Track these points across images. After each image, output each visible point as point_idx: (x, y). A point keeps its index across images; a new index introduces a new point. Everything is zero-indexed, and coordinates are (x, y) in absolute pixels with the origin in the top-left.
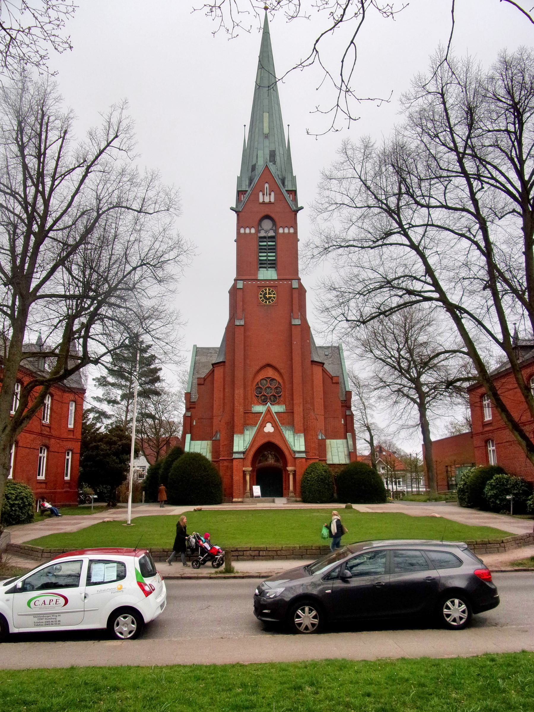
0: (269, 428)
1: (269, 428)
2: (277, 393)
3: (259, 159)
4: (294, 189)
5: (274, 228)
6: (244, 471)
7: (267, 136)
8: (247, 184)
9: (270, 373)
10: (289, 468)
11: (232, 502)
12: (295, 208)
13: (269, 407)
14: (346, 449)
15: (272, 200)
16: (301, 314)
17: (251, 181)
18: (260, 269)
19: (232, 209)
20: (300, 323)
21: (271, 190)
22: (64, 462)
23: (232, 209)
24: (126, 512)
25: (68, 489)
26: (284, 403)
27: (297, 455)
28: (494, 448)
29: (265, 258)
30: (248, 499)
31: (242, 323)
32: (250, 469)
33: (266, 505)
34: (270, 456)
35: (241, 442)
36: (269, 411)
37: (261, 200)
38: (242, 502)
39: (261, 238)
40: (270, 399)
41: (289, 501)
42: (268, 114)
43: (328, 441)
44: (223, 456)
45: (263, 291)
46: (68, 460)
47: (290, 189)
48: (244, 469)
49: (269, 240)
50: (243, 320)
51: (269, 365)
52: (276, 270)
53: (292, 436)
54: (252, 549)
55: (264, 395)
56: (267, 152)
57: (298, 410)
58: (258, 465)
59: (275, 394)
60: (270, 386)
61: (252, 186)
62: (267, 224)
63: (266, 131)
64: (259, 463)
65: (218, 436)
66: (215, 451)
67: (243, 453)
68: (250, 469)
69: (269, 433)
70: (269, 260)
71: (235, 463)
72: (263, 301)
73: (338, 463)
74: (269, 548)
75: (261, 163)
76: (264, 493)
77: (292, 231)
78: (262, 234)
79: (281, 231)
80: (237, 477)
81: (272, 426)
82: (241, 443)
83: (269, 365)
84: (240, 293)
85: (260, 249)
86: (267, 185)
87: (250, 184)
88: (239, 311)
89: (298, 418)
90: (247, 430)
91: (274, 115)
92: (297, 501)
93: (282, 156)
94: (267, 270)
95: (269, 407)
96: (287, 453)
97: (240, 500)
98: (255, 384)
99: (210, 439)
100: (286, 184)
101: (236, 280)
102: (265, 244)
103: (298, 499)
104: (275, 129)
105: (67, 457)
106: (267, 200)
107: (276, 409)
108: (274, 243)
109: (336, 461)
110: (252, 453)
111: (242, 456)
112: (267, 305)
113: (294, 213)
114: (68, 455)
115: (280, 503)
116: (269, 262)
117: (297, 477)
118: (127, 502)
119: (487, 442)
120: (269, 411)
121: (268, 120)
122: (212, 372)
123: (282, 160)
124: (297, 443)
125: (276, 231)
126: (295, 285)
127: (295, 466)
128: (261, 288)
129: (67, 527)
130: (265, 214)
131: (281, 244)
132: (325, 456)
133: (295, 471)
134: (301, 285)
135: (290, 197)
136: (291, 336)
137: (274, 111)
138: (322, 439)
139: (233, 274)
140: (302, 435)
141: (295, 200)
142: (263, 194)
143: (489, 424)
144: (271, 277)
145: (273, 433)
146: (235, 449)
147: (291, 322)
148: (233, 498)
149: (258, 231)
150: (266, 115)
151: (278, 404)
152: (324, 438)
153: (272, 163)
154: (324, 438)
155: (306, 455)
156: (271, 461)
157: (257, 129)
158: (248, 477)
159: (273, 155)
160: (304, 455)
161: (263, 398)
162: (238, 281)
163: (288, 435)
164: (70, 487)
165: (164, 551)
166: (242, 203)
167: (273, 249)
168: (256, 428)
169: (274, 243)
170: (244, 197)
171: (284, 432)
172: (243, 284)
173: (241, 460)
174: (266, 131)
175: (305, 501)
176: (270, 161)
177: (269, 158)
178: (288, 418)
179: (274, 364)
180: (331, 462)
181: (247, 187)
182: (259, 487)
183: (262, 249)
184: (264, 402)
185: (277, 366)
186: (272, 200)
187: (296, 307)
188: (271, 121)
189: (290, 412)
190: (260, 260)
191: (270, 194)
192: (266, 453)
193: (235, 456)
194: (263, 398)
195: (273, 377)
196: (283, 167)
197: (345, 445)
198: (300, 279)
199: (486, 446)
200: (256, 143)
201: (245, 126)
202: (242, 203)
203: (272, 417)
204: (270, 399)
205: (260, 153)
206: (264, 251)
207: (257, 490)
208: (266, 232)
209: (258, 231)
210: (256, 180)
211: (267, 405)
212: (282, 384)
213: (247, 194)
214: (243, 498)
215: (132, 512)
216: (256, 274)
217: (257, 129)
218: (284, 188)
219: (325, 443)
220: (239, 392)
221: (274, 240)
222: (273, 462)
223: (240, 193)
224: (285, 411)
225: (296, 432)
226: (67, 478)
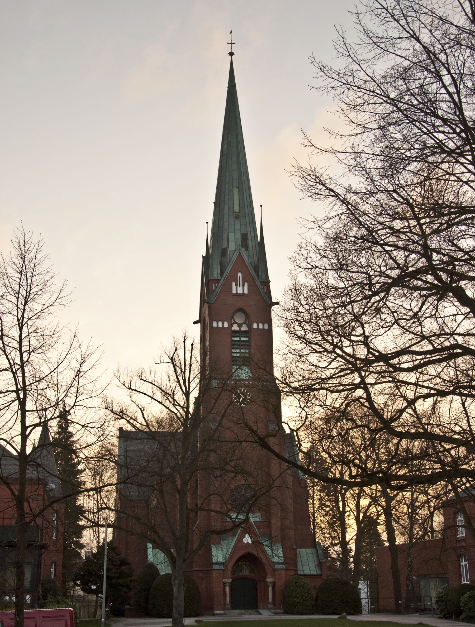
0: (247, 539)
3: (230, 243)
5: (247, 322)
7: (237, 216)
8: (219, 272)
10: (269, 580)
11: (214, 614)
14: (316, 559)
27: (277, 567)
28: (467, 563)
34: (245, 567)
37: (234, 291)
38: (224, 614)
48: (224, 580)
56: (239, 235)
61: (224, 275)
63: (237, 209)
68: (230, 580)
71: (215, 575)
77: (266, 327)
78: (235, 327)
79: (255, 326)
82: (219, 555)
89: (276, 528)
97: (222, 612)
100: (260, 274)
102: (238, 339)
103: (280, 611)
106: (240, 291)
108: (247, 339)
109: (307, 572)
110: (231, 564)
111: (222, 567)
119: (459, 557)
124: (276, 555)
125: (250, 326)
127: (274, 578)
133: (274, 583)
142: (236, 285)
143: (463, 540)
153: (244, 249)
156: (246, 572)
168: (235, 539)
169: (247, 339)
173: (221, 572)
174: (237, 209)
175: (287, 612)
176: (243, 247)
180: (302, 573)
181: (219, 275)
183: (234, 345)
186: (246, 292)
188: (241, 199)
189: (267, 522)
190: (233, 357)
191: (243, 285)
199: (459, 562)
205: (231, 236)
206: (236, 347)
209: (231, 325)
214: (224, 610)
224: (261, 520)
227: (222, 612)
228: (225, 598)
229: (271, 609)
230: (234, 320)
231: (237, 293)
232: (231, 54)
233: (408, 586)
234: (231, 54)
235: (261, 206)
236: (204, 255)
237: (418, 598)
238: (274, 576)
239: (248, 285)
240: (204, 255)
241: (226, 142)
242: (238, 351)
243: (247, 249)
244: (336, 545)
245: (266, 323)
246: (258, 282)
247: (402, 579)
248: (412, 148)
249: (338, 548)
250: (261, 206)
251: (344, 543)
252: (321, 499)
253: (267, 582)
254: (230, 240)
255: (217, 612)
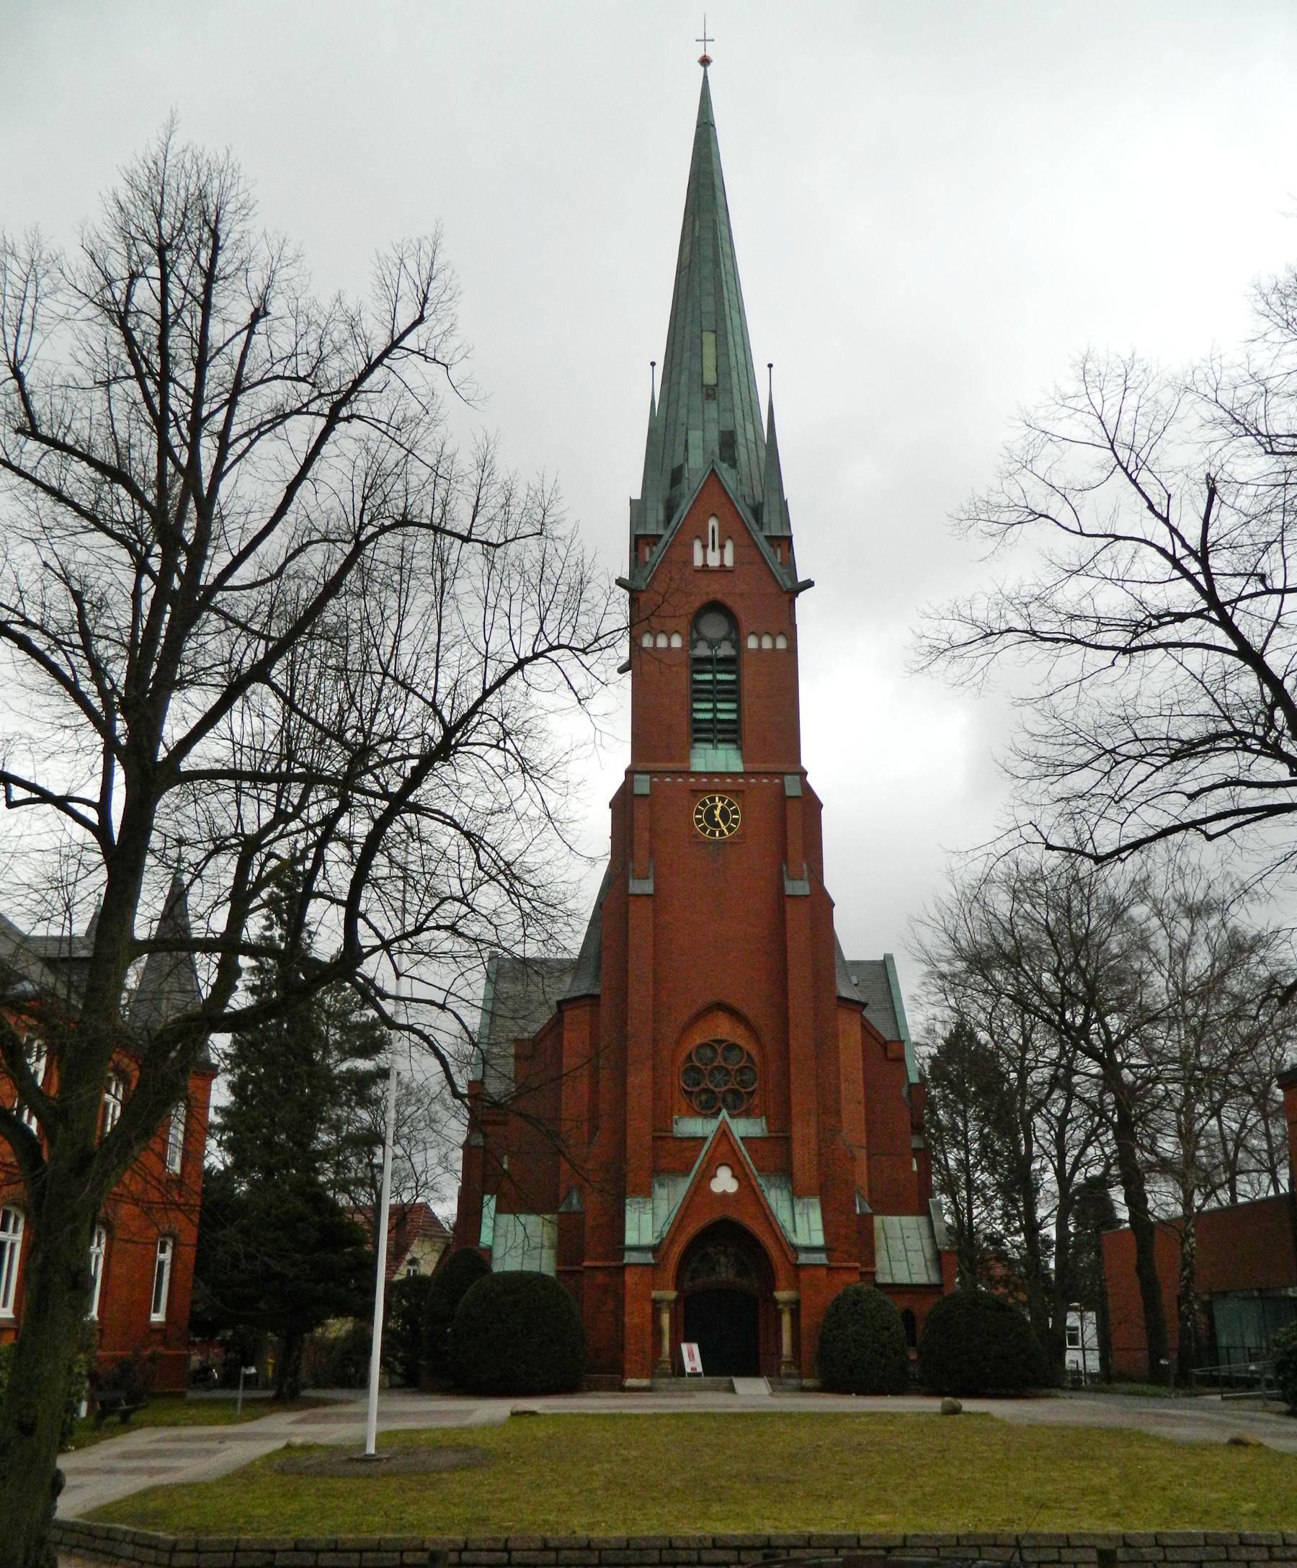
0: (724, 1182)
1: (724, 1182)
2: (743, 1084)
3: (692, 452)
4: (786, 534)
5: (733, 636)
6: (655, 1302)
7: (710, 393)
8: (661, 516)
9: (724, 1028)
10: (782, 1295)
12: (789, 584)
13: (724, 1122)
14: (927, 1242)
15: (729, 562)
16: (810, 870)
17: (670, 509)
18: (697, 745)
19: (620, 582)
20: (807, 892)
21: (725, 535)
22: (149, 1267)
23: (620, 582)
24: (363, 1417)
25: (161, 1350)
26: (764, 1112)
27: (803, 1258)
29: (709, 716)
30: (666, 1380)
31: (647, 887)
32: (672, 1295)
33: (711, 1401)
34: (723, 1260)
35: (647, 1218)
36: (724, 1133)
37: (698, 562)
39: (699, 660)
40: (724, 1100)
41: (778, 1386)
42: (712, 336)
43: (878, 1220)
44: (595, 1259)
45: (704, 804)
46: (162, 1264)
47: (776, 532)
48: (655, 1294)
49: (721, 668)
50: (651, 880)
51: (721, 1007)
52: (740, 748)
53: (787, 1204)
54: (815, 1544)
55: (707, 1090)
56: (713, 435)
57: (804, 1132)
58: (687, 1284)
59: (736, 1086)
60: (723, 1064)
61: (673, 523)
62: (714, 627)
63: (710, 377)
64: (692, 1279)
65: (575, 1201)
66: (569, 1245)
67: (654, 1249)
68: (672, 1295)
69: (725, 1194)
70: (708, 701)
71: (630, 1278)
72: (704, 829)
73: (906, 1281)
74: (869, 1537)
75: (696, 462)
76: (714, 1365)
78: (702, 650)
79: (752, 643)
80: (635, 1316)
81: (734, 1176)
82: (644, 1224)
83: (721, 1007)
84: (641, 814)
85: (696, 691)
86: (713, 523)
87: (668, 519)
88: (641, 853)
89: (803, 1156)
90: (661, 1185)
91: (730, 337)
92: (803, 1389)
93: (752, 446)
94: (715, 748)
95: (724, 1122)
96: (774, 1253)
97: (645, 1382)
98: (684, 1055)
99: (553, 1210)
100: (765, 519)
101: (629, 773)
102: (709, 677)
104: (734, 374)
105: (161, 1256)
106: (713, 560)
107: (742, 1128)
109: (902, 1277)
110: (677, 1250)
111: (649, 1258)
112: (717, 841)
113: (787, 598)
114: (163, 1251)
115: (752, 1392)
116: (719, 727)
117: (804, 1323)
118: (363, 1383)
120: (724, 1133)
121: (713, 349)
122: (557, 1023)
123: (754, 457)
124: (805, 1226)
125: (738, 644)
126: (792, 789)
128: (700, 795)
129: (182, 1463)
130: (705, 598)
131: (752, 679)
132: (872, 1263)
133: (798, 1302)
134: (807, 789)
135: (775, 553)
136: (783, 922)
137: (729, 329)
138: (863, 1215)
139: (622, 758)
140: (816, 1201)
141: (790, 564)
142: (705, 547)
144: (727, 766)
145: (735, 1194)
146: (631, 1238)
147: (781, 887)
148: (623, 1377)
149: (691, 644)
150: (709, 339)
151: (747, 1114)
152: (870, 1211)
153: (725, 465)
154: (870, 1211)
155: (828, 1258)
156: (725, 1273)
157: (684, 378)
158: (665, 1319)
159: (728, 442)
160: (821, 1258)
161: (704, 1097)
162: (637, 777)
163: (777, 1200)
164: (165, 1343)
165: (546, 1547)
166: (649, 568)
167: (732, 692)
170: (652, 553)
171: (766, 1194)
172: (651, 783)
175: (832, 1386)
176: (723, 460)
177: (717, 451)
178: (775, 1155)
179: (732, 1001)
180: (888, 1280)
181: (661, 525)
182: (695, 1347)
183: (699, 692)
184: (708, 1110)
185: (745, 1011)
186: (729, 562)
187: (794, 850)
190: (695, 721)
191: (722, 547)
192: (710, 1250)
193: (630, 1258)
194: (704, 1097)
195: (731, 1040)
196: (756, 475)
197: (925, 1232)
198: (806, 773)
200: (683, 412)
201: (653, 364)
202: (649, 568)
203: (734, 1151)
204: (724, 1100)
205: (695, 437)
206: (704, 696)
207: (691, 1356)
208: (711, 647)
210: (684, 508)
211: (720, 1118)
212: (757, 1059)
213: (661, 544)
214: (652, 1375)
215: (381, 1416)
216: (686, 758)
217: (684, 378)
218: (761, 529)
219: (872, 1221)
220: (639, 1079)
221: (734, 668)
222: (731, 1276)
223: (639, 542)
224: (766, 1134)
225: (796, 1194)
226: (157, 1317)
227: (645, 1382)
228: (658, 1343)
229: (789, 1376)
230: (699, 633)
231: (705, 565)
232: (705, 61)
233: (1183, 1318)
234: (705, 61)
235: (770, 366)
236: (637, 496)
237: (1211, 1350)
238: (795, 1285)
239: (735, 547)
240: (637, 496)
241: (687, 242)
242: (710, 706)
243: (733, 464)
244: (1017, 1232)
245: (781, 633)
246: (760, 538)
247: (1168, 1297)
248: (1146, 670)
249: (1020, 1238)
250: (770, 366)
251: (1032, 1228)
252: (983, 1137)
253: (775, 1302)
254: (690, 446)
255: (630, 1382)
